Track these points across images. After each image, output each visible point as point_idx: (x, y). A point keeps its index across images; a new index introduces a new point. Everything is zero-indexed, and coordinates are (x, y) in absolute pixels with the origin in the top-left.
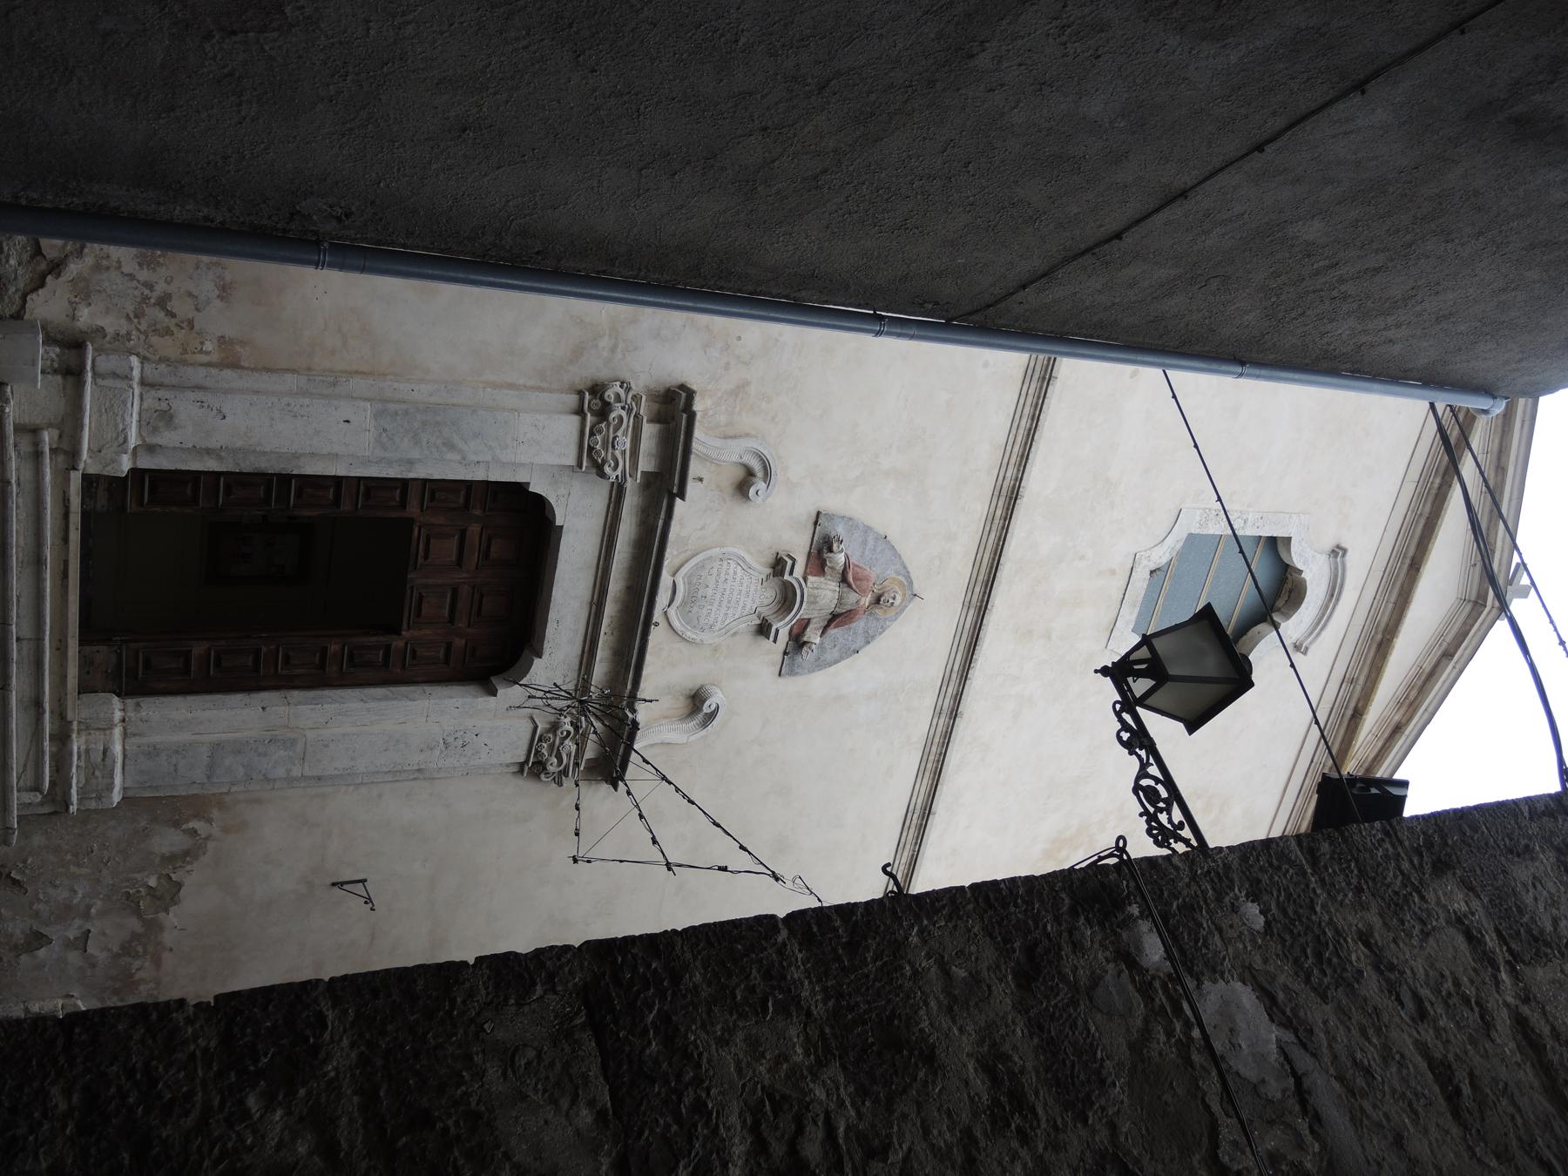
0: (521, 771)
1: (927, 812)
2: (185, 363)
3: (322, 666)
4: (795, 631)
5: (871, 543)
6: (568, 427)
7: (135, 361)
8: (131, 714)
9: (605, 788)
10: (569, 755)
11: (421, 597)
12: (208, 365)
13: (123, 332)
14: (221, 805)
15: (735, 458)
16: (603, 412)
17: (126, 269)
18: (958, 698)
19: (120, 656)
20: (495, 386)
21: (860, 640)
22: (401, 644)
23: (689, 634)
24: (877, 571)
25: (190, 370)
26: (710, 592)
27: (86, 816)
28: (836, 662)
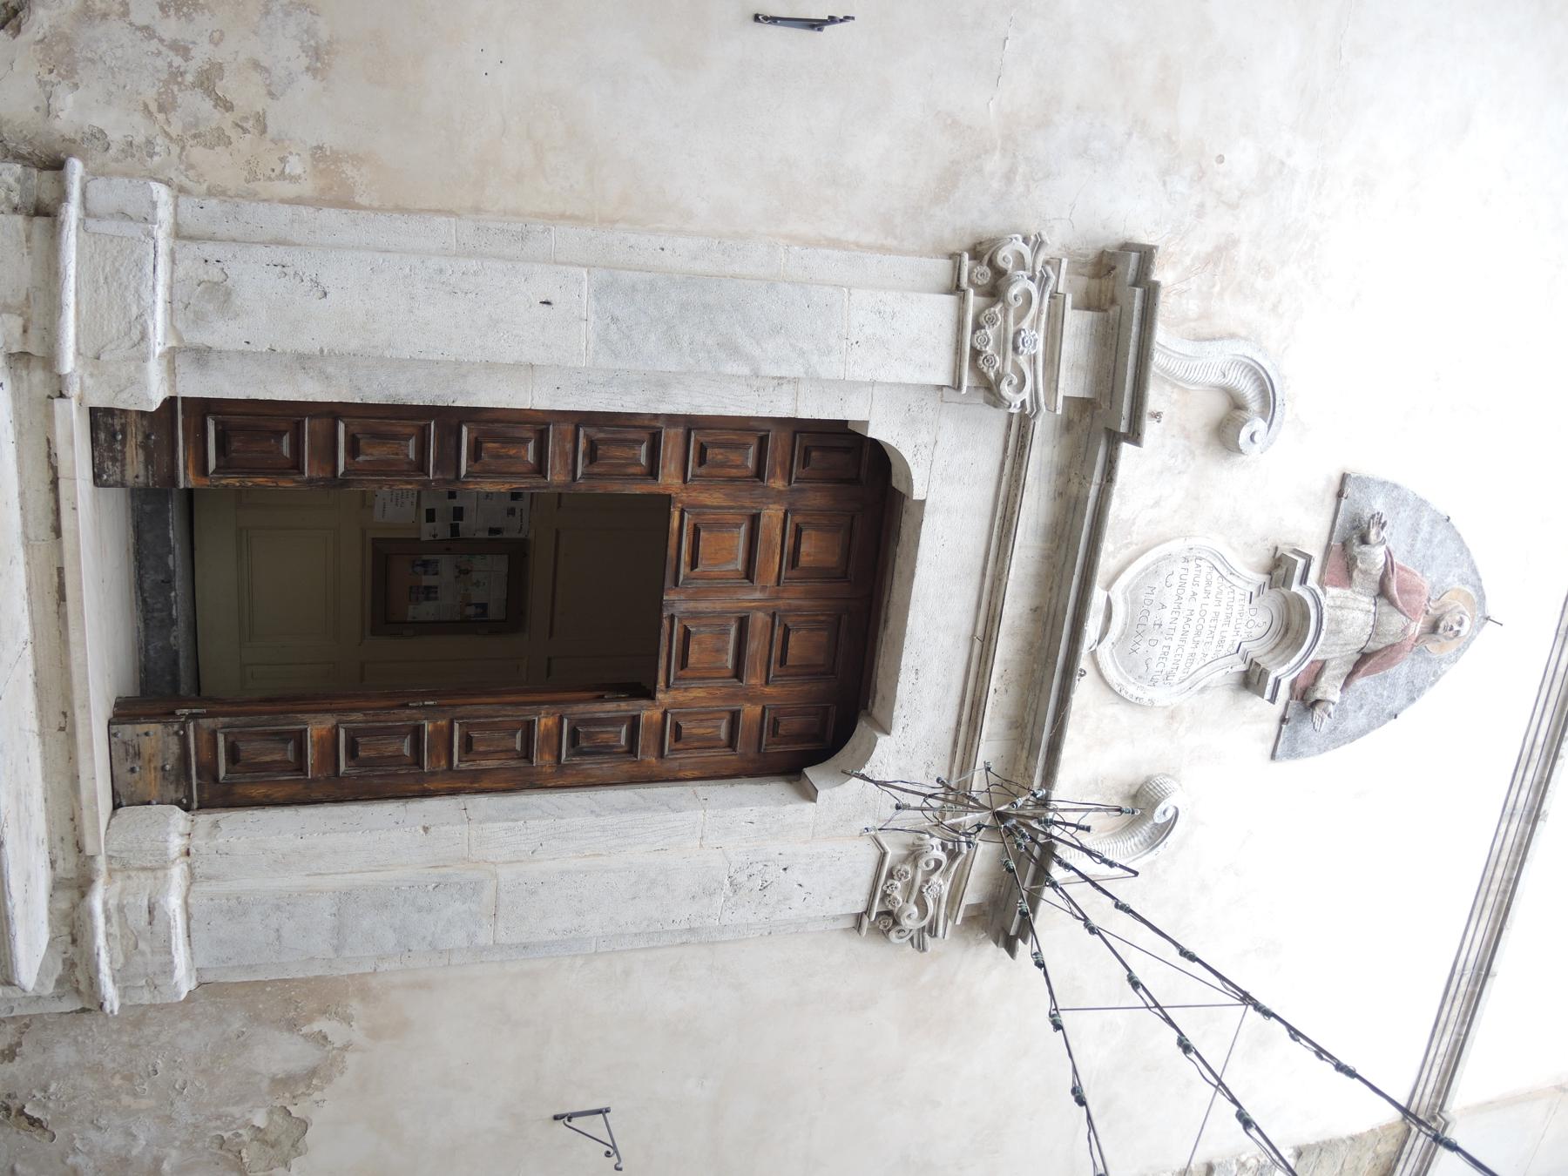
0: (858, 926)
1: (1483, 972)
2: (253, 196)
3: (527, 754)
4: (1300, 684)
5: (1425, 528)
6: (932, 317)
7: (161, 193)
8: (199, 842)
9: (992, 952)
10: (938, 901)
11: (687, 634)
12: (298, 201)
13: (139, 139)
14: (365, 993)
15: (1215, 378)
16: (995, 291)
17: (139, 18)
18: (1541, 788)
19: (184, 741)
20: (807, 243)
21: (1401, 696)
22: (657, 714)
23: (1132, 690)
24: (1432, 577)
25: (262, 208)
26: (1166, 616)
27: (136, 1017)
28: (1363, 733)
